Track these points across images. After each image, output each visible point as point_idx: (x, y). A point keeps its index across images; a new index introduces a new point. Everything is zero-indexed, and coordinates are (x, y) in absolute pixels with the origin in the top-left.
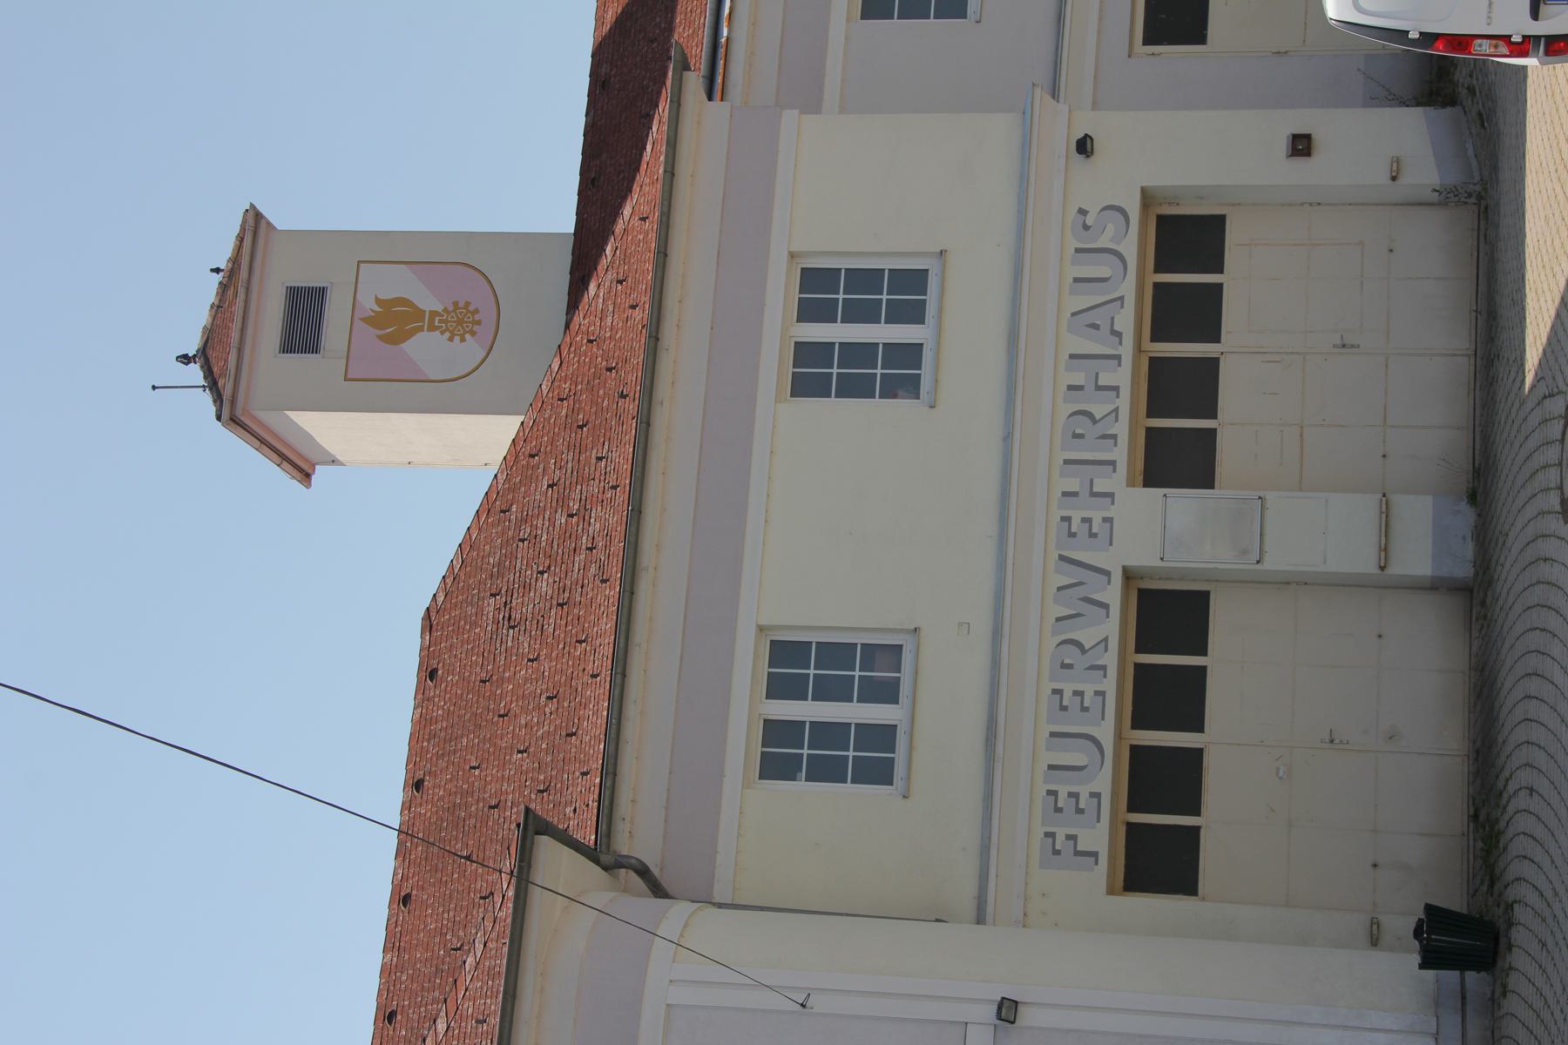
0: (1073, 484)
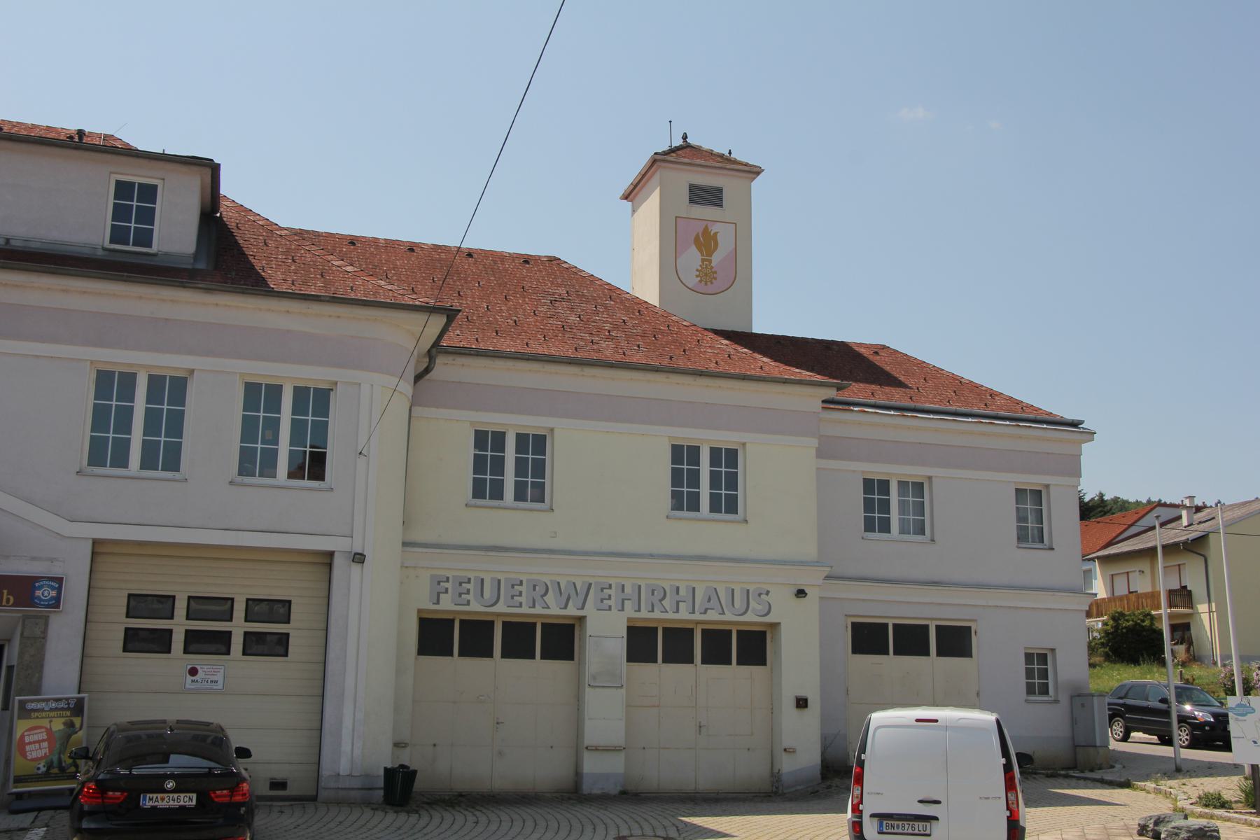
0: (628, 590)
